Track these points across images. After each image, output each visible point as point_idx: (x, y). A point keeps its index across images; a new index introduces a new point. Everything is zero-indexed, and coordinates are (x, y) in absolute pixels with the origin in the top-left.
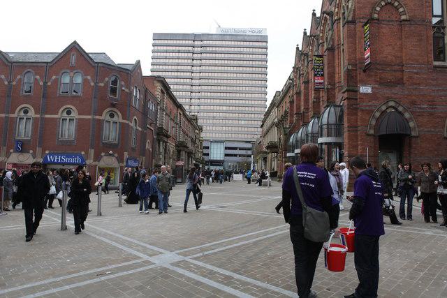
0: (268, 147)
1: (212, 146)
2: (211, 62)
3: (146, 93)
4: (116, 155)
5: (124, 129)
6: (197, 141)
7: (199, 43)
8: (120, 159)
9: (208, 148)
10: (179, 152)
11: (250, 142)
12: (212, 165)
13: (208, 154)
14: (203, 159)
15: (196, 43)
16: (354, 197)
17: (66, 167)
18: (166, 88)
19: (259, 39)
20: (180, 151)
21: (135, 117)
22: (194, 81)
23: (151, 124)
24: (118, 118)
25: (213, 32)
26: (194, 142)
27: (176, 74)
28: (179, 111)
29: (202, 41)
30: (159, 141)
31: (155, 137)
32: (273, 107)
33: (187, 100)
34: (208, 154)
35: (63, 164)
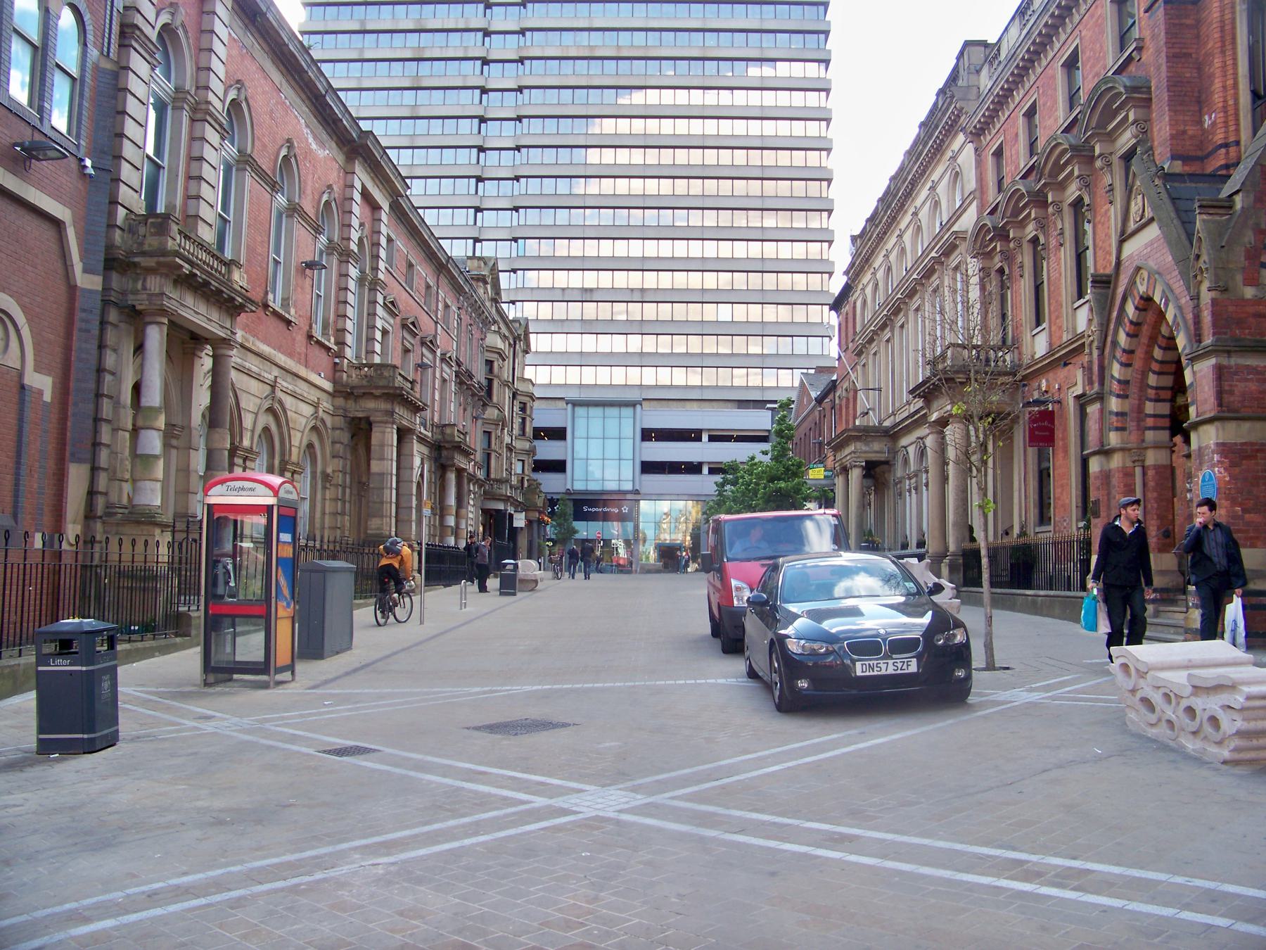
1: (581, 423)
6: (502, 395)
9: (558, 434)
10: (360, 430)
11: (760, 404)
12: (580, 516)
14: (534, 487)
26: (478, 393)
28: (362, 177)
33: (462, 217)
34: (558, 466)
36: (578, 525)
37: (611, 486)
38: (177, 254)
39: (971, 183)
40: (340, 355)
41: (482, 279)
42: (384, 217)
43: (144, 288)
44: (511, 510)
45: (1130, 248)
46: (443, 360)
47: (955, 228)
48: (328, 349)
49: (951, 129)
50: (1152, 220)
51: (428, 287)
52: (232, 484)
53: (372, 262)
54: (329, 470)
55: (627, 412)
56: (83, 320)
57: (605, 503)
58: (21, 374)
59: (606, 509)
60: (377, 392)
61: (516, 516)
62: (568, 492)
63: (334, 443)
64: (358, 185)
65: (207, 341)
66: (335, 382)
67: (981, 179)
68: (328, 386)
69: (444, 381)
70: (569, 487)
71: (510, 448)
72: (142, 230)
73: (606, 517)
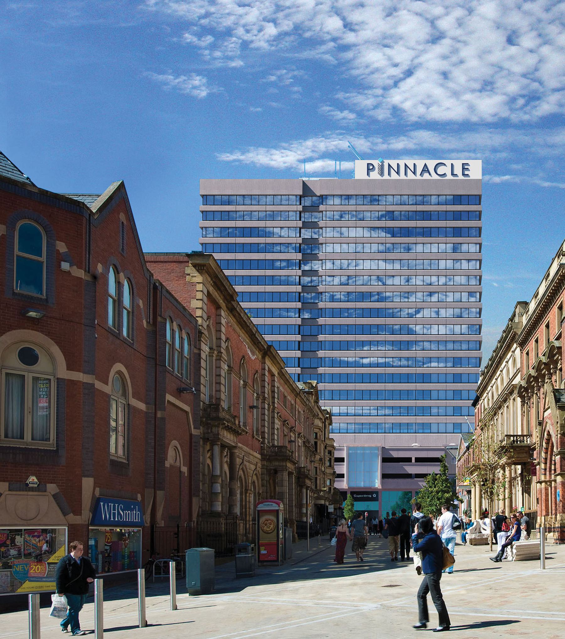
0: (503, 450)
3: (156, 299)
4: (52, 488)
6: (321, 447)
8: (68, 501)
17: (392, 578)
18: (223, 294)
20: (276, 472)
23: (179, 392)
26: (312, 449)
31: (194, 432)
32: (509, 347)
35: (390, 577)
38: (224, 419)
39: (519, 366)
40: (263, 443)
41: (311, 393)
42: (223, 313)
43: (212, 432)
44: (327, 503)
45: (546, 414)
47: (513, 383)
48: (259, 441)
49: (513, 340)
50: (549, 408)
51: (292, 405)
52: (265, 503)
53: (261, 389)
56: (195, 446)
58: (180, 468)
61: (329, 507)
64: (267, 368)
65: (227, 447)
66: (262, 454)
67: (522, 363)
68: (259, 456)
69: (299, 446)
71: (324, 473)
72: (209, 410)
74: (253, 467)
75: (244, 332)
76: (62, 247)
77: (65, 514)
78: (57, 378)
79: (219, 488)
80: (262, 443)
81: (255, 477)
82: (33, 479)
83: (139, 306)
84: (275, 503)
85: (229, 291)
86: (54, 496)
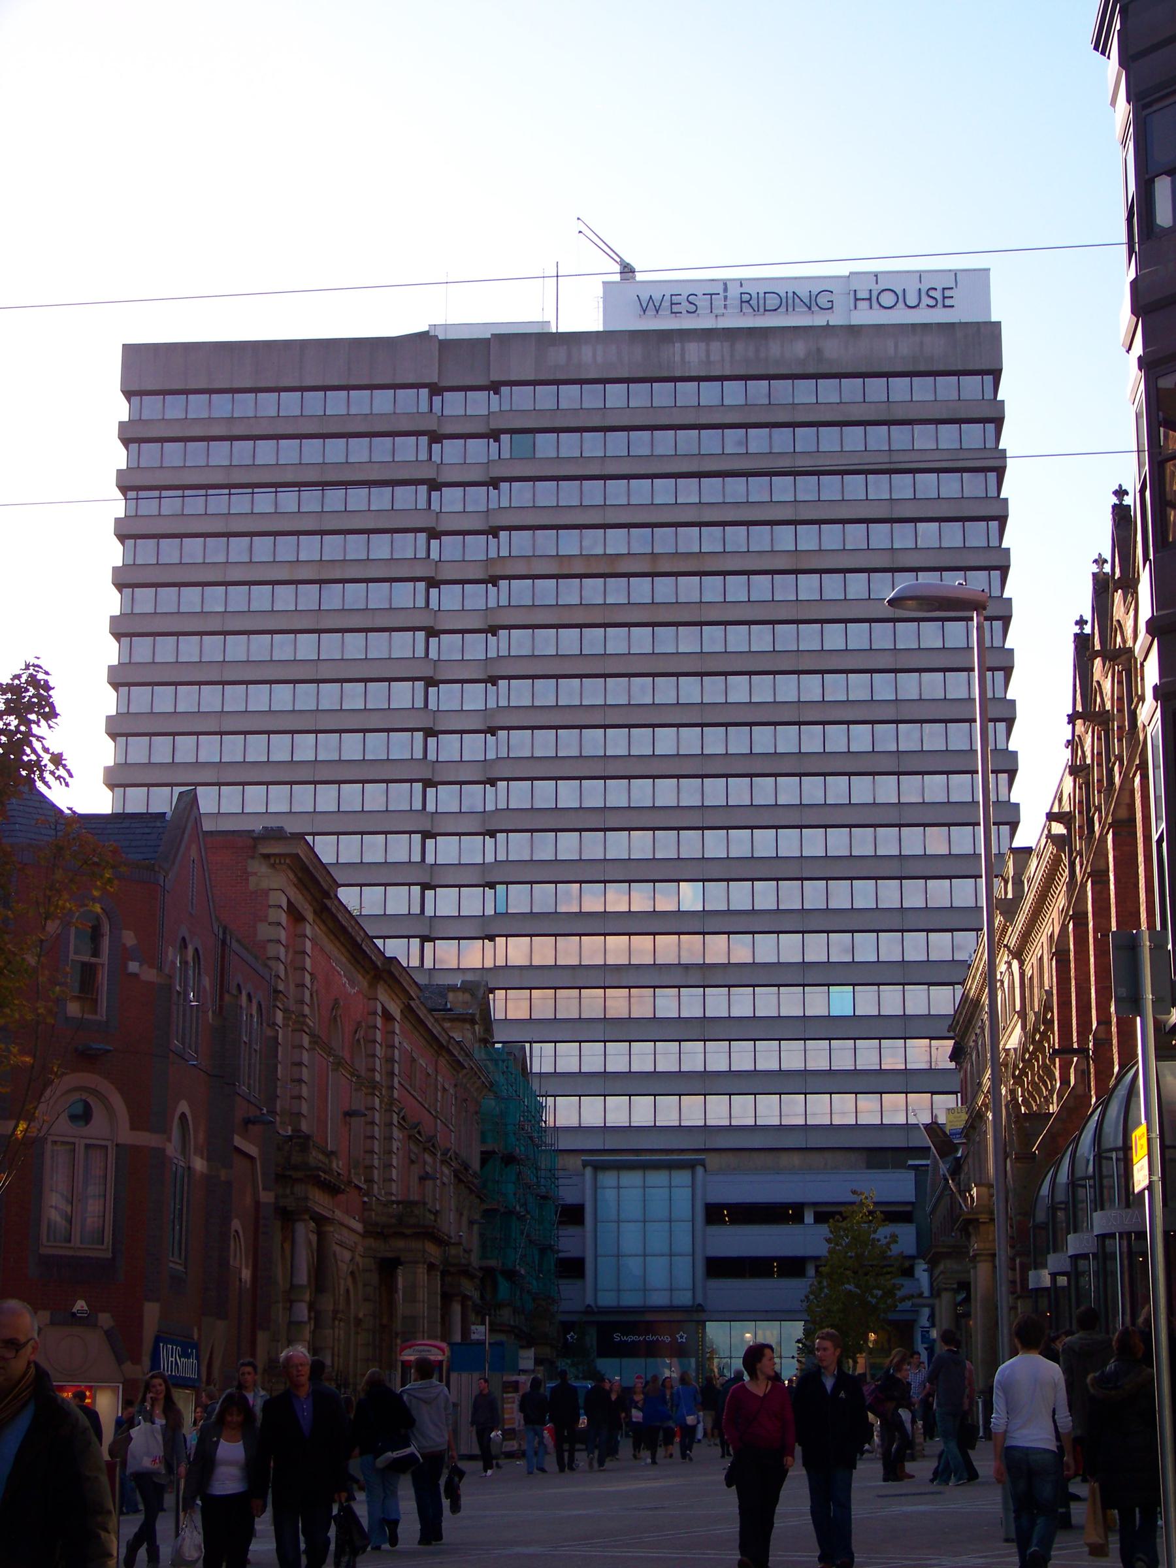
2: (570, 543)
4: (105, 1320)
5: (137, 1172)
7: (479, 403)
12: (610, 1349)
13: (574, 1268)
15: (453, 403)
16: (208, 1160)
19: (936, 350)
21: (184, 1107)
22: (447, 697)
24: (113, 1124)
25: (582, 313)
27: (306, 646)
29: (494, 387)
30: (287, 1217)
36: (605, 1365)
37: (659, 1299)
43: (292, 1193)
46: (442, 1162)
54: (361, 1315)
55: (682, 1177)
57: (650, 1327)
59: (650, 1338)
60: (408, 1231)
62: (589, 1310)
63: (365, 1285)
66: (363, 1221)
68: (358, 1226)
70: (589, 1300)
73: (651, 1351)
74: (347, 1255)
75: (338, 944)
76: (129, 938)
77: (120, 1362)
78: (117, 1145)
79: (306, 1312)
80: (367, 1194)
81: (350, 1280)
82: (80, 1305)
83: (204, 987)
84: (435, 1346)
85: (323, 883)
86: (108, 1334)
